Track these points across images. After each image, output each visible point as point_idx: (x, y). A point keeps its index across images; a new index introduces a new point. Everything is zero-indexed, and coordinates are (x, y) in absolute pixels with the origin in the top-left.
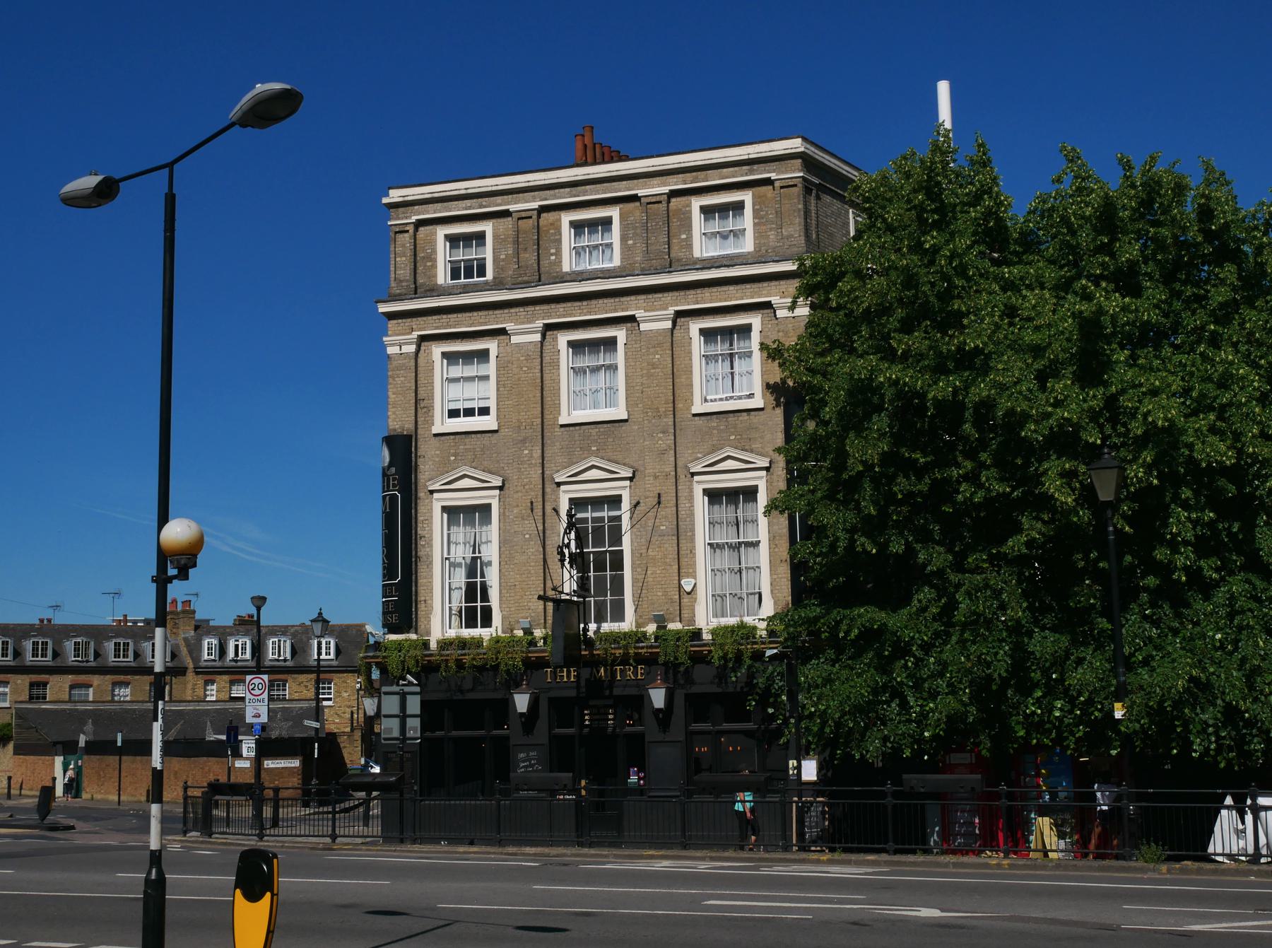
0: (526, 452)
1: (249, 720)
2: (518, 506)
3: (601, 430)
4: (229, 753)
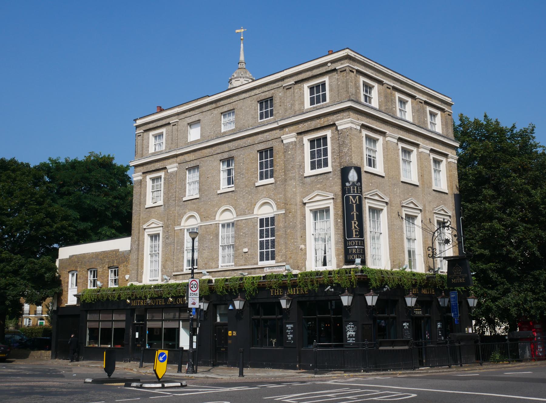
0: (395, 190)
1: (190, 306)
4: (242, 58)
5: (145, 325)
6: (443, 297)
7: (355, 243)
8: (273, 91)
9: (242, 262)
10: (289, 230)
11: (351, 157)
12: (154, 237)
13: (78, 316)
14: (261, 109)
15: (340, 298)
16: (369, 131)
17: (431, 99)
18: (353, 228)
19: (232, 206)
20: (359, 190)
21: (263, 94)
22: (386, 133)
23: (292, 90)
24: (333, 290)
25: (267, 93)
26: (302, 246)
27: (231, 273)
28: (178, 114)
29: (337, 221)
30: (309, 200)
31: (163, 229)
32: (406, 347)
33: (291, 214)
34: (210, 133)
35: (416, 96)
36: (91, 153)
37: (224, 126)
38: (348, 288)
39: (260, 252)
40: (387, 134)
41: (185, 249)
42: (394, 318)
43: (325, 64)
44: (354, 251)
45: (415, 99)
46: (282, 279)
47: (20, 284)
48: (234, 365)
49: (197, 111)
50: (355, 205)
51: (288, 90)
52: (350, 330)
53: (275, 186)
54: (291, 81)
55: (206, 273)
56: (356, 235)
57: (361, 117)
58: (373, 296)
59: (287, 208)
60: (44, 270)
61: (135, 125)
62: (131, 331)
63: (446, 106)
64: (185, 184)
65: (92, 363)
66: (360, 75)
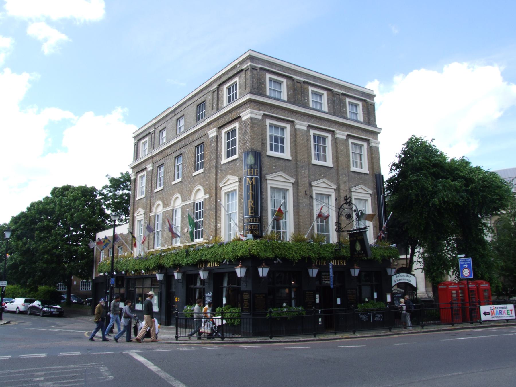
0: (303, 171)
4: (224, 302)
8: (205, 96)
15: (235, 270)
16: (274, 120)
21: (200, 100)
29: (241, 201)
33: (212, 197)
49: (165, 120)
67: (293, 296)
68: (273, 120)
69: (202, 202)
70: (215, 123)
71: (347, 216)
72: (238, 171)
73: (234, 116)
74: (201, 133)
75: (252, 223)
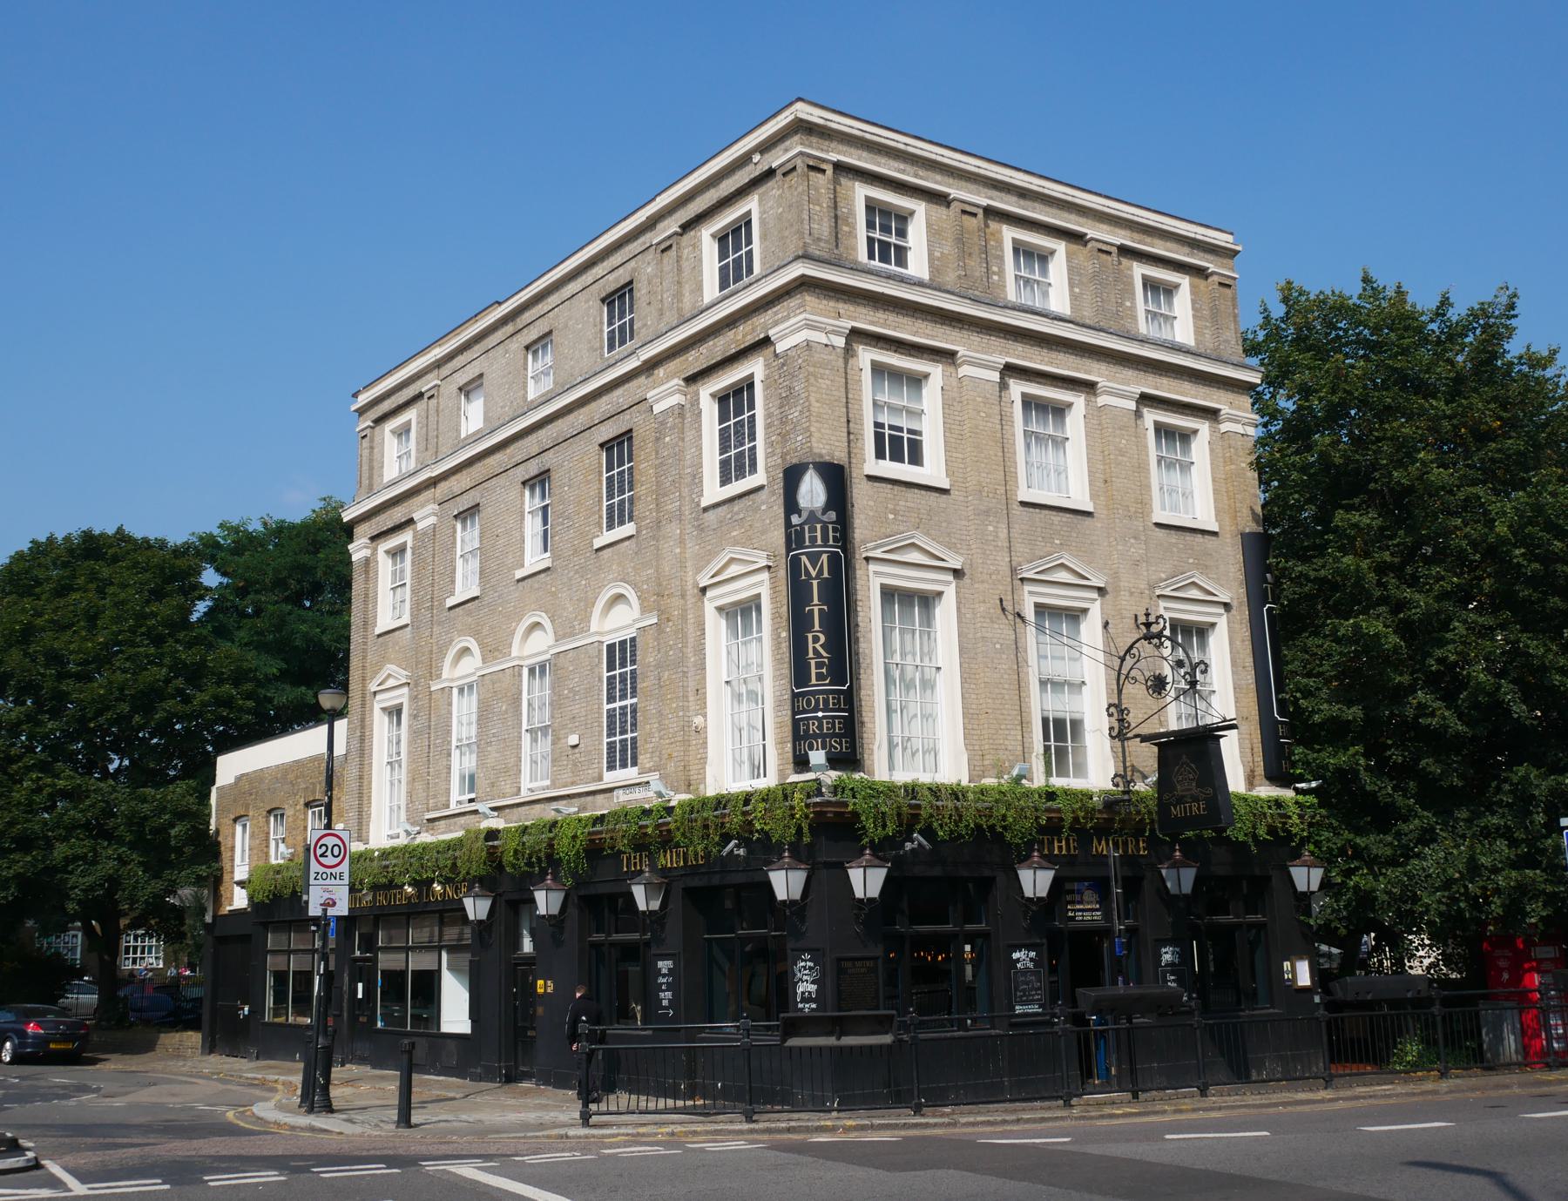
0: (991, 528)
1: (314, 910)
2: (984, 602)
3: (1064, 519)
5: (375, 960)
6: (1176, 865)
7: (817, 701)
8: (633, 264)
9: (566, 776)
10: (667, 673)
11: (808, 434)
12: (395, 712)
13: (245, 939)
14: (610, 323)
15: (768, 877)
17: (1148, 240)
18: (811, 654)
19: (546, 612)
20: (831, 534)
21: (611, 277)
22: (957, 352)
23: (672, 252)
24: (742, 852)
25: (621, 270)
26: (698, 720)
27: (544, 809)
28: (438, 364)
29: (779, 637)
30: (713, 577)
31: (410, 690)
32: (887, 1039)
33: (670, 624)
34: (502, 407)
35: (1086, 234)
36: (325, 499)
37: (536, 382)
38: (790, 844)
39: (608, 743)
40: (959, 355)
41: (454, 743)
42: (1261, 926)
43: (744, 160)
44: (813, 728)
45: (1085, 244)
46: (640, 823)
47: (106, 858)
48: (561, 1083)
49: (478, 349)
50: (815, 583)
51: (665, 254)
52: (805, 978)
53: (637, 544)
54: (671, 226)
55: (488, 812)
56: (820, 677)
57: (852, 308)
58: (865, 867)
59: (663, 608)
60: (167, 817)
61: (353, 408)
62: (346, 979)
63: (1211, 257)
64: (453, 561)
65: (271, 1067)
66: (857, 180)
67: (969, 969)
68: (882, 348)
69: (633, 640)
70: (673, 365)
71: (1149, 683)
72: (764, 532)
73: (744, 336)
74: (620, 397)
75: (823, 711)
